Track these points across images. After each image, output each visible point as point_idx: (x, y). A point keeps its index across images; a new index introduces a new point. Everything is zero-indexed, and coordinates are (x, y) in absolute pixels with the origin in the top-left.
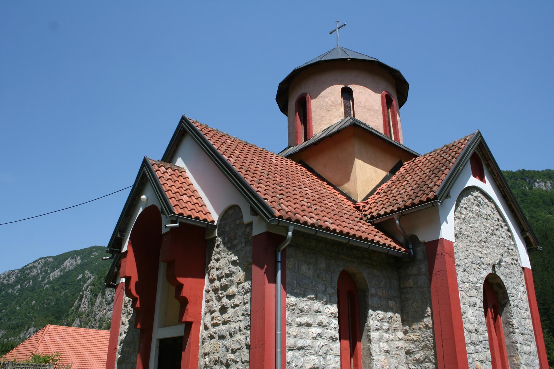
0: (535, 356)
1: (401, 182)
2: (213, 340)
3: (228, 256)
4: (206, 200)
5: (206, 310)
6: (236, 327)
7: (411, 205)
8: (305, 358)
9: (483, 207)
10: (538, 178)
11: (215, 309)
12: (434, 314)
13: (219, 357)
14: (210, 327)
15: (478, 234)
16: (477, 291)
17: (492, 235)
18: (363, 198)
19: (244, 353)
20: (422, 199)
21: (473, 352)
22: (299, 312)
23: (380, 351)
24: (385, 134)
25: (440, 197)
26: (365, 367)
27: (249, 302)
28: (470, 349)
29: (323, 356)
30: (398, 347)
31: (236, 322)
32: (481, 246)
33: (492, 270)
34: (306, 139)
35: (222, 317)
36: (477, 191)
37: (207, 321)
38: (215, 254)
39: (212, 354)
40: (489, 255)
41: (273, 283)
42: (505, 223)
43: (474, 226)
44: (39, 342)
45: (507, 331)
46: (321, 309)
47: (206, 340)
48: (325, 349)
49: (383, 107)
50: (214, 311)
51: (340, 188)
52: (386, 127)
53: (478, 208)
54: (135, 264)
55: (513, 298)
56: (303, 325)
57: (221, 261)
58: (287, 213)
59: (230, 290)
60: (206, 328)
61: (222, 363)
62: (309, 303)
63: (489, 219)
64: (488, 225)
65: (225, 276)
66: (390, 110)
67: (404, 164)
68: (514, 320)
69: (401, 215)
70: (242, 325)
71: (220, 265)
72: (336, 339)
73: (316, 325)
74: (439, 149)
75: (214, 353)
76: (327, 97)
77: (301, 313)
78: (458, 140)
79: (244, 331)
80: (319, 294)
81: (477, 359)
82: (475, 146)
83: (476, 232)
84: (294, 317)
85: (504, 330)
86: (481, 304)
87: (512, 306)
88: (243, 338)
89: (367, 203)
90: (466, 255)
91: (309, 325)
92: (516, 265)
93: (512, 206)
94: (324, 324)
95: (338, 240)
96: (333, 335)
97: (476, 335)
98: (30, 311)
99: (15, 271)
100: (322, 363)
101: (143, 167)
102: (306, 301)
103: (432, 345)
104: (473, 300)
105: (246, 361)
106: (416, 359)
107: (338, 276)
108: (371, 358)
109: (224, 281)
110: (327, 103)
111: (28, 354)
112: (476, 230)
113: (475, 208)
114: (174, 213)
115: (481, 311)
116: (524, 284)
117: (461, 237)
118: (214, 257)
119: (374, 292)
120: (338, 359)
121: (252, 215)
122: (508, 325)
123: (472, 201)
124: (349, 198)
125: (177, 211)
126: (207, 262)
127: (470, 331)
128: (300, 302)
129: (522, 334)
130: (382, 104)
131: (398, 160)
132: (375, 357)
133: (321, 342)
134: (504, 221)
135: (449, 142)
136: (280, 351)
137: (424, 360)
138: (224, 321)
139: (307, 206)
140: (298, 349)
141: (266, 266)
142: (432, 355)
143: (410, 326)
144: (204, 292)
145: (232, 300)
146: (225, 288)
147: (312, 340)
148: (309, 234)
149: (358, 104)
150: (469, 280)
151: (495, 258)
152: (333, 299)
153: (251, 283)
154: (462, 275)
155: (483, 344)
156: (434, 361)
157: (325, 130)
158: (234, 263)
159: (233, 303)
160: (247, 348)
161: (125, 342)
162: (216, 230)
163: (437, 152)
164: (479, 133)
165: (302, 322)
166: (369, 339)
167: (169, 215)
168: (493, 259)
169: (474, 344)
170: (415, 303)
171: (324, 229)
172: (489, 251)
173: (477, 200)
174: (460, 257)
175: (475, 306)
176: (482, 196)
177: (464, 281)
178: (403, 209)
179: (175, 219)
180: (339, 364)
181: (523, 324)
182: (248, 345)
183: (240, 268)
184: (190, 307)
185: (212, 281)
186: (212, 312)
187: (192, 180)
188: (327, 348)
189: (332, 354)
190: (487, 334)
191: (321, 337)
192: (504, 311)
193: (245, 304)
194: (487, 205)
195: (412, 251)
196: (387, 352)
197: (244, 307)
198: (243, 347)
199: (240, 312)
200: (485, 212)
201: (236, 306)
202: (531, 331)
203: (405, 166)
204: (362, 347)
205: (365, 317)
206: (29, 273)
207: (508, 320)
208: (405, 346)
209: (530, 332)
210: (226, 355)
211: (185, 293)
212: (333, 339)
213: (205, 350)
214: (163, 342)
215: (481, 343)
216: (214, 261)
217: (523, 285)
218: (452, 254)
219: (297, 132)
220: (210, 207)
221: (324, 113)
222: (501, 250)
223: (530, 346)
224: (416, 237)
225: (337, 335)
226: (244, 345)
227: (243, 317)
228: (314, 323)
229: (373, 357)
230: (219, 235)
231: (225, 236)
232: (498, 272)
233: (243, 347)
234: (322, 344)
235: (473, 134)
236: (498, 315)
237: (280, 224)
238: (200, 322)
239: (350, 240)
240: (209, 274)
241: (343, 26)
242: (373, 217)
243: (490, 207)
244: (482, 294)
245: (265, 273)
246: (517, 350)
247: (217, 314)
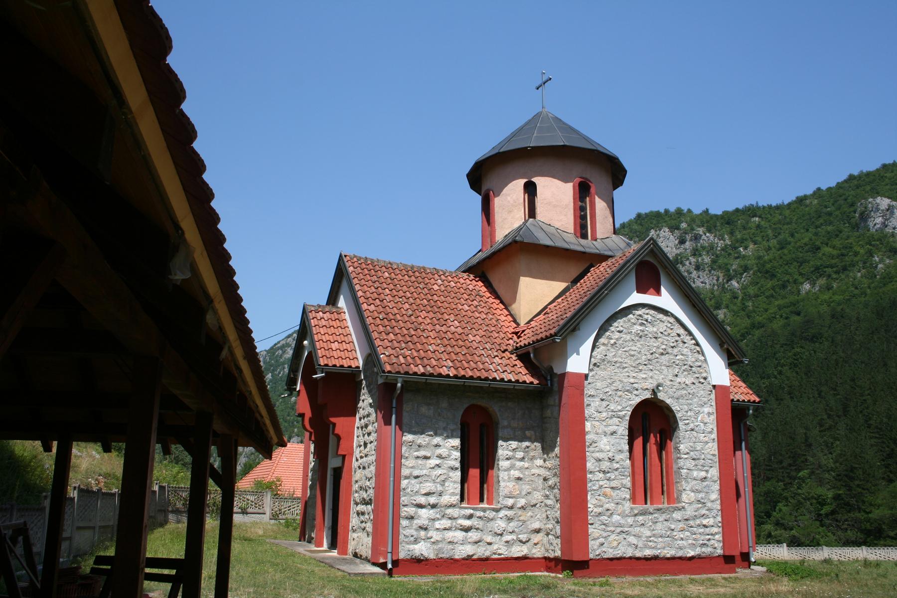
14: (359, 459)
36: (643, 308)
44: (275, 465)
48: (442, 478)
49: (574, 199)
62: (427, 439)
68: (682, 445)
72: (457, 469)
76: (509, 195)
84: (411, 451)
98: (289, 412)
99: (262, 353)
107: (461, 413)
111: (251, 480)
112: (633, 353)
133: (439, 471)
134: (690, 333)
144: (356, 429)
147: (430, 470)
161: (313, 470)
188: (445, 477)
196: (519, 479)
206: (281, 355)
212: (452, 469)
234: (440, 473)
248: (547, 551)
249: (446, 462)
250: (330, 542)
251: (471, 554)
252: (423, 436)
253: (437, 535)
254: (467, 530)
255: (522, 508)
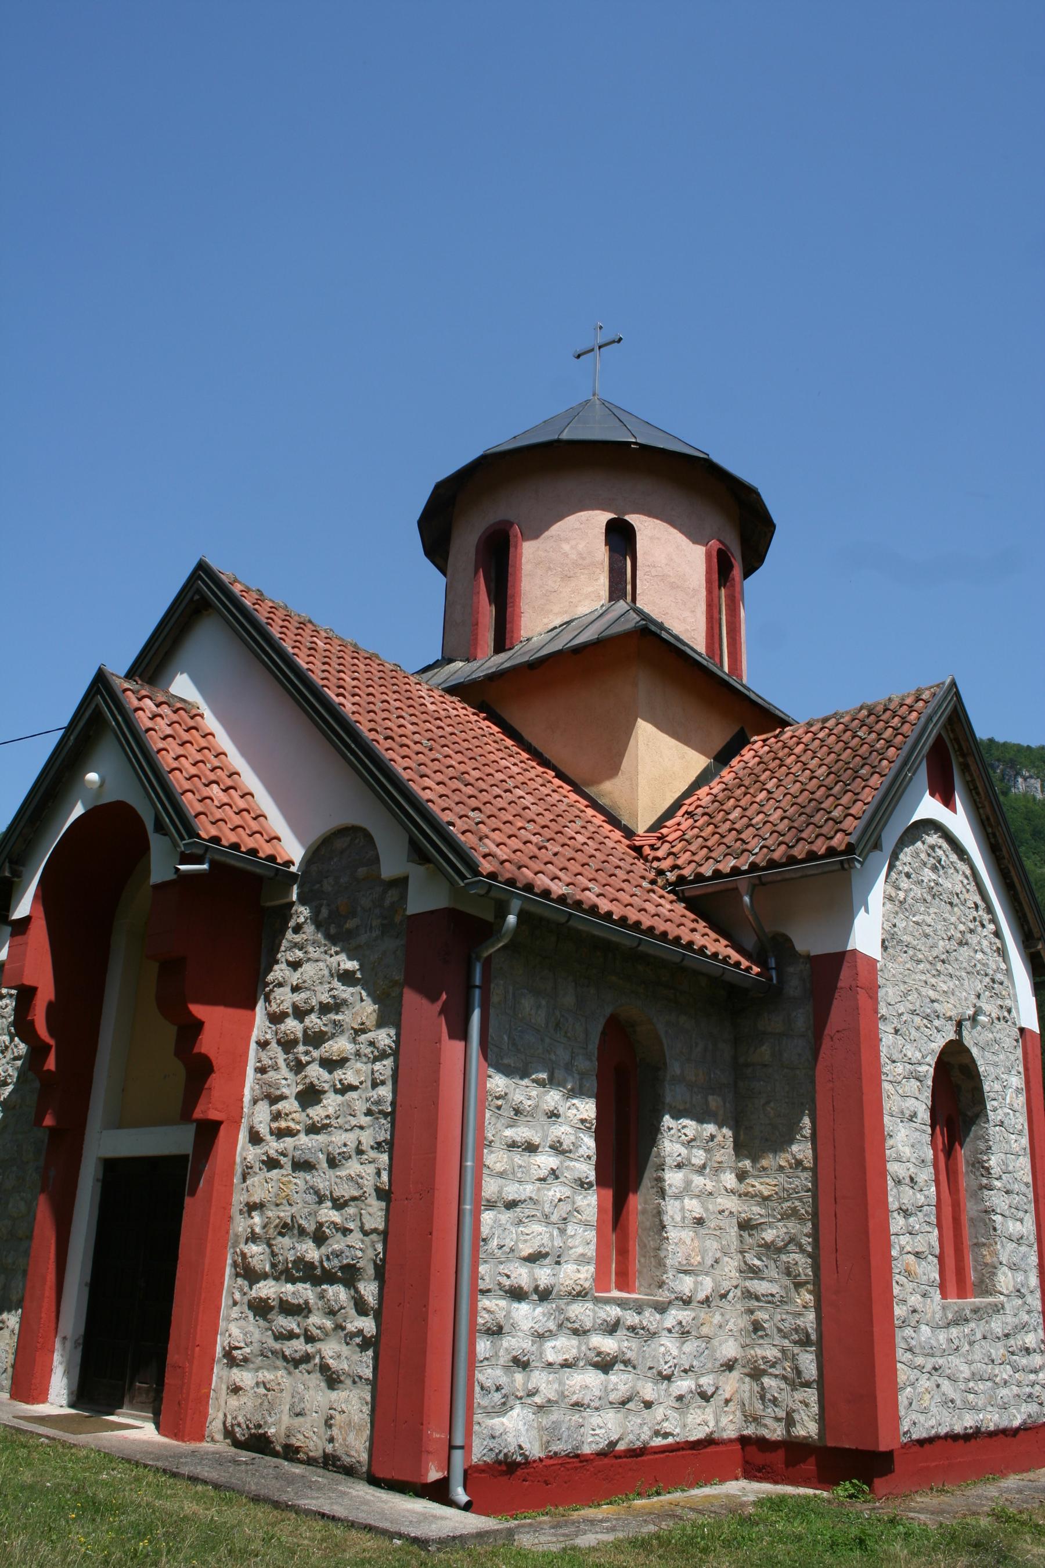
0: (1030, 1246)
1: (751, 791)
2: (275, 1171)
3: (327, 957)
4: (264, 801)
5: (258, 1092)
6: (349, 1143)
7: (784, 860)
8: (521, 1229)
9: (945, 873)
10: (1026, 767)
11: (286, 1091)
12: (819, 1134)
13: (293, 1217)
14: (268, 1137)
15: (930, 942)
16: (919, 1084)
17: (961, 944)
18: (651, 823)
19: (370, 1210)
20: (814, 848)
21: (902, 1231)
22: (512, 1113)
23: (684, 1218)
24: (707, 655)
25: (861, 847)
26: (645, 1257)
27: (389, 1083)
28: (897, 1223)
29: (560, 1226)
30: (723, 1211)
31: (346, 1130)
32: (934, 972)
33: (955, 1032)
34: (500, 646)
35: (304, 1114)
37: (261, 1122)
38: (290, 949)
39: (273, 1208)
40: (951, 996)
41: (460, 1039)
42: (990, 916)
43: (924, 920)
45: (974, 1184)
46: (559, 1108)
47: (254, 1170)
48: (565, 1208)
49: (709, 581)
50: (282, 1098)
51: (591, 791)
52: (713, 636)
53: (934, 877)
54: (49, 952)
55: (995, 1103)
56: (519, 1147)
57: (308, 969)
58: (502, 862)
59: (331, 1046)
60: (255, 1138)
61: (302, 1232)
62: (534, 1093)
63: (956, 905)
64: (953, 919)
65: (317, 1008)
66: (723, 590)
67: (752, 740)
68: (993, 1158)
69: (757, 882)
70: (367, 1138)
71: (304, 978)
73: (547, 1149)
74: (847, 713)
75: (277, 1205)
76: (567, 540)
77: (515, 1117)
78: (900, 695)
79: (373, 1154)
80: (556, 1071)
81: (908, 1248)
82: (943, 718)
83: (927, 936)
84: (499, 1125)
85: (967, 1181)
86: (925, 1116)
87: (992, 1123)
88: (369, 1171)
89: (662, 838)
90: (902, 994)
91: (531, 1148)
92: (1007, 1022)
93: (1009, 872)
94: (565, 1147)
95: (597, 932)
96: (585, 1175)
97: (911, 1191)
100: (556, 1244)
101: (94, 696)
102: (527, 1087)
103: (809, 1210)
104: (911, 1104)
105: (375, 1231)
106: (766, 1242)
107: (600, 1028)
108: (661, 1235)
109: (313, 1021)
110: (567, 556)
112: (928, 930)
113: (928, 875)
114: (199, 836)
115: (924, 1132)
116: (1021, 1069)
117: (894, 947)
118: (285, 955)
119: (678, 1071)
120: (592, 1235)
121: (413, 862)
122: (978, 1170)
123: (923, 856)
124: (613, 821)
125: (206, 830)
126: (263, 966)
127: (899, 1182)
128: (515, 1089)
129: (1007, 1192)
130: (707, 573)
131: (735, 729)
132: (672, 1234)
133: (556, 1191)
134: (990, 909)
135: (876, 696)
136: (471, 1210)
137: (786, 1245)
138: (313, 1124)
139: (536, 844)
140: (505, 1207)
141: (444, 996)
142: (806, 1235)
143: (755, 1160)
144: (253, 1046)
145: (339, 1074)
146: (316, 1039)
147: (538, 1184)
148: (541, 919)
149: (647, 569)
150: (905, 1055)
151: (964, 1003)
152: (587, 1084)
153: (398, 1035)
154: (890, 1043)
155: (924, 1212)
156: (809, 1249)
157: (555, 628)
158: (346, 978)
159: (340, 1081)
160: (379, 1198)
162: (295, 887)
163: (842, 720)
164: (953, 684)
165: (518, 1139)
166: (661, 1188)
167: (183, 839)
168: (958, 1006)
169: (905, 1211)
170: (772, 1104)
171: (584, 911)
172: (951, 984)
173: (933, 854)
174: (888, 993)
175: (914, 1119)
176: (945, 846)
177: (894, 1057)
178: (764, 869)
179: (199, 851)
180: (593, 1247)
181: (1011, 1168)
182: (383, 1190)
183: (363, 992)
184: (216, 1082)
185: (276, 1018)
186: (274, 1099)
187: (223, 741)
188: (569, 1208)
189: (580, 1223)
190: (933, 1189)
191: (557, 1178)
192: (972, 1135)
193: (375, 1085)
194: (955, 868)
195: (774, 974)
196: (700, 1222)
197: (374, 1094)
198: (367, 1195)
199: (358, 1101)
200: (950, 886)
201: (345, 1089)
202: (1027, 1184)
203: (755, 747)
204: (639, 1207)
205: (653, 1133)
207: (979, 1156)
208: (740, 1209)
209: (1024, 1189)
210: (316, 1213)
211: (207, 1044)
213: (250, 1196)
214: (111, 1167)
215: (920, 1211)
216: (284, 966)
217: (1019, 1073)
218: (872, 990)
219: (477, 624)
220: (277, 822)
221: (555, 582)
222: (977, 982)
223: (1021, 1221)
224: (788, 940)
225: (592, 1177)
226: (370, 1189)
227: (369, 1118)
228: (543, 1144)
229: (666, 1233)
230: (303, 900)
231: (321, 905)
232: (968, 1040)
233: (367, 1195)
234: (558, 1196)
235: (938, 686)
236: (957, 1144)
237: (493, 894)
238: (238, 1123)
239: (493, 887)
240: (267, 1000)
241: (614, 342)
242: (681, 880)
243: (961, 873)
244: (930, 1091)
245: (440, 1013)
246: (995, 1229)
247: (289, 1105)
248: (756, 1420)
249: (568, 1163)
250: (75, 1387)
251: (614, 1437)
252: (526, 1082)
253: (549, 1382)
254: (605, 1365)
255: (707, 1301)
